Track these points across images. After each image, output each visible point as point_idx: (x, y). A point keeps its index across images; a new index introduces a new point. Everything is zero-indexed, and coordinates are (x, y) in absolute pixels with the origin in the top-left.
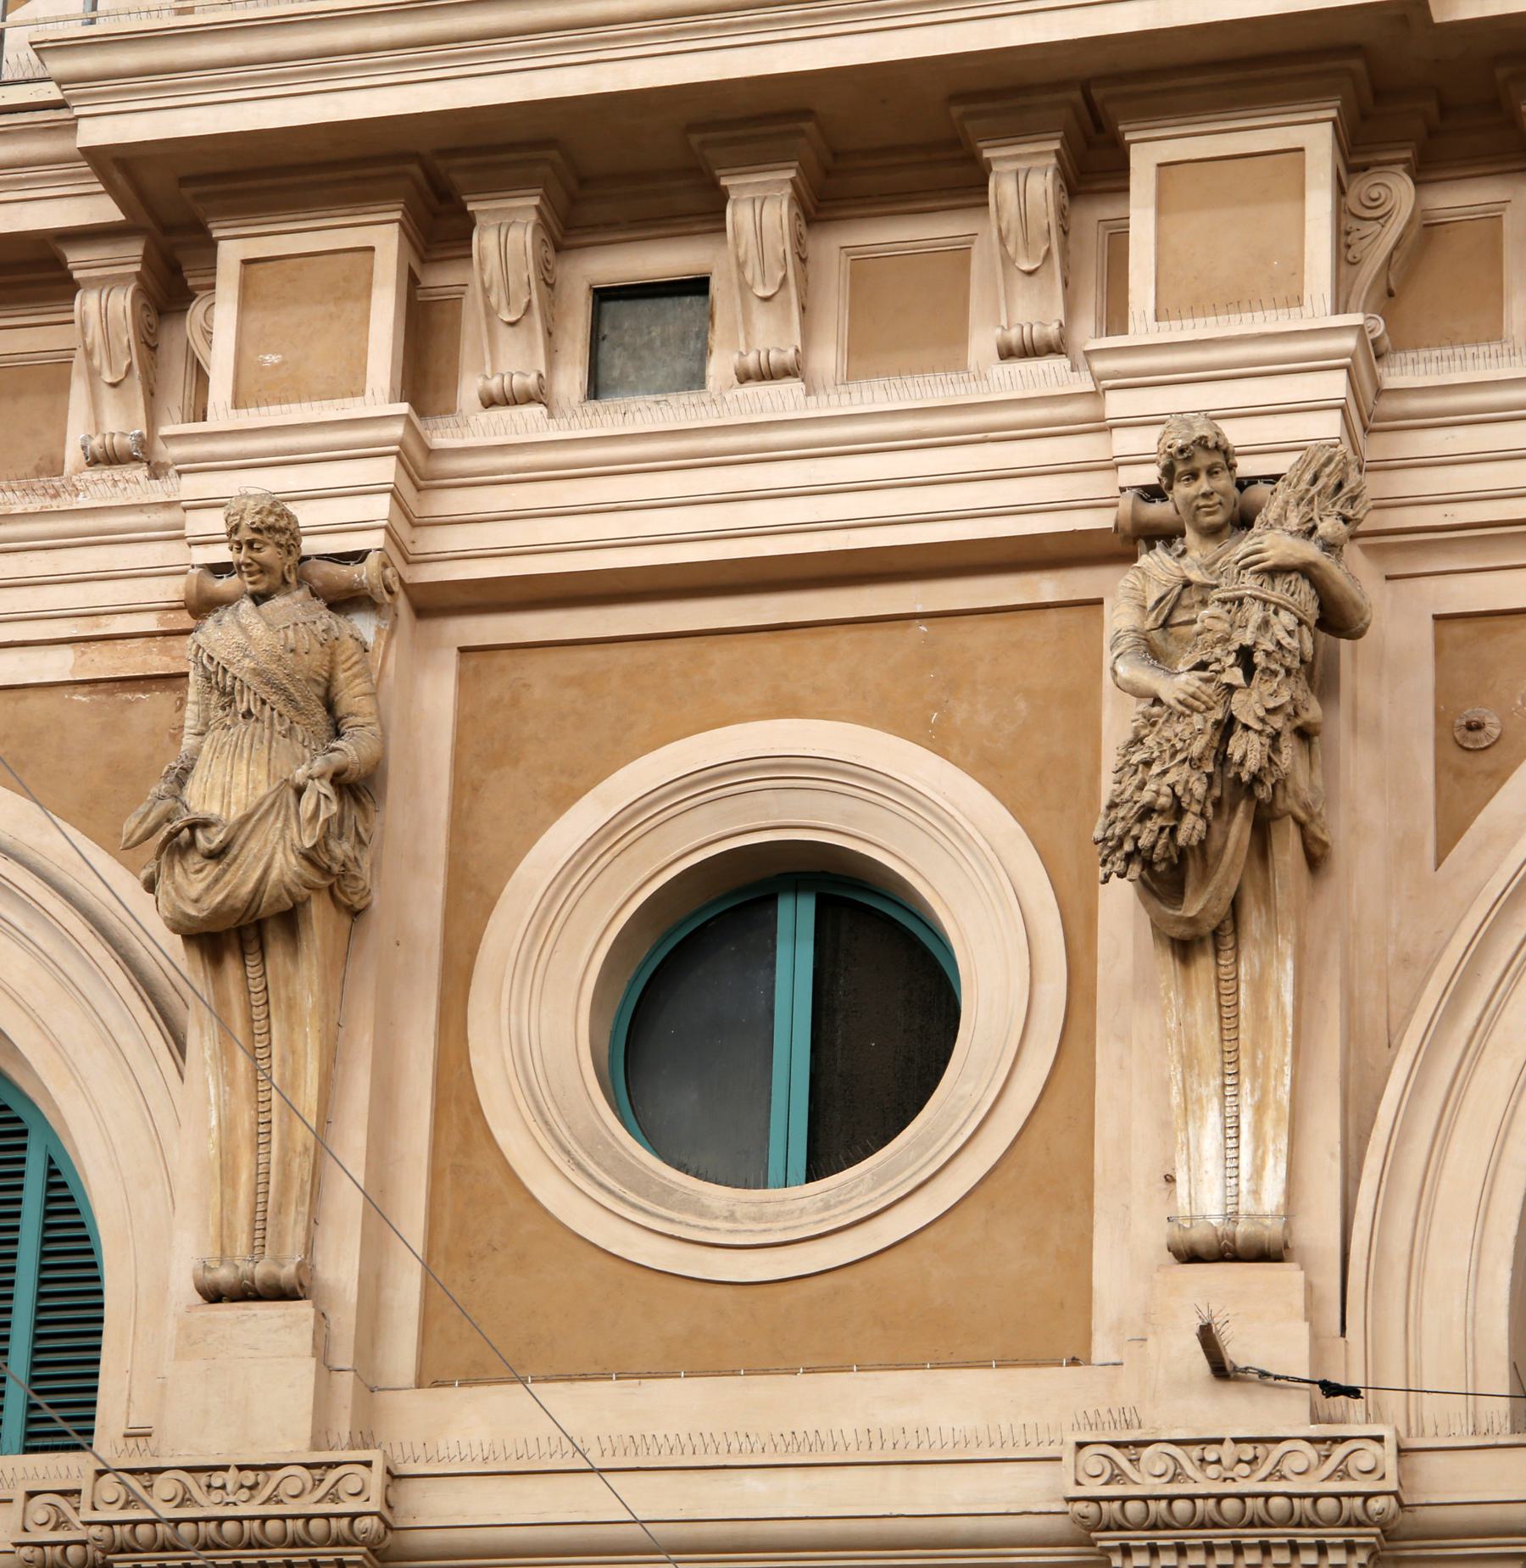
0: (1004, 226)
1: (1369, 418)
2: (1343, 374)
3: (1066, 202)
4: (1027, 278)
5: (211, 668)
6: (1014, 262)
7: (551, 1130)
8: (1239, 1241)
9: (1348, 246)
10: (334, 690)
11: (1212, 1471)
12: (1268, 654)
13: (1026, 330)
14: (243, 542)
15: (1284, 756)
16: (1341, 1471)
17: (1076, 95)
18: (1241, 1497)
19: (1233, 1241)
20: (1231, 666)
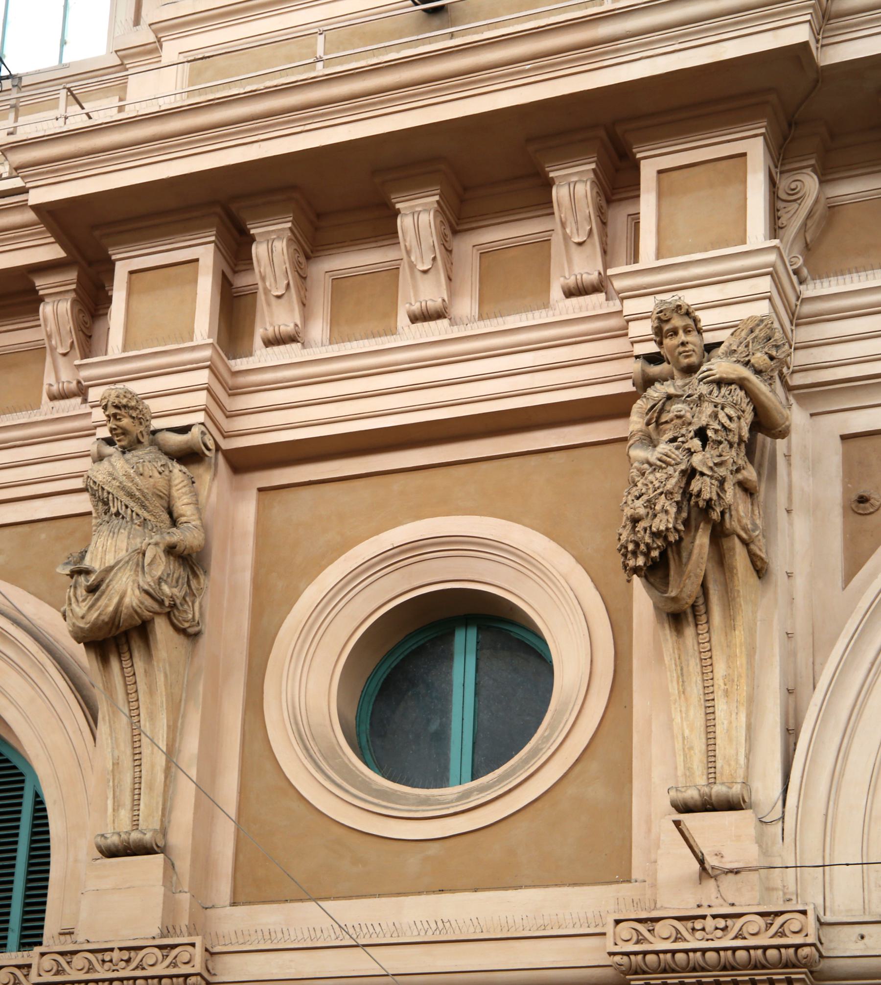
0: (407, 244)
2: (769, 278)
3: (604, 203)
4: (580, 248)
5: (95, 488)
6: (570, 238)
7: (311, 756)
8: (713, 798)
9: (779, 218)
10: (172, 503)
11: (699, 935)
12: (716, 431)
13: (579, 277)
14: (110, 415)
15: (728, 494)
16: (780, 932)
17: (602, 133)
18: (717, 950)
19: (710, 796)
20: (691, 438)
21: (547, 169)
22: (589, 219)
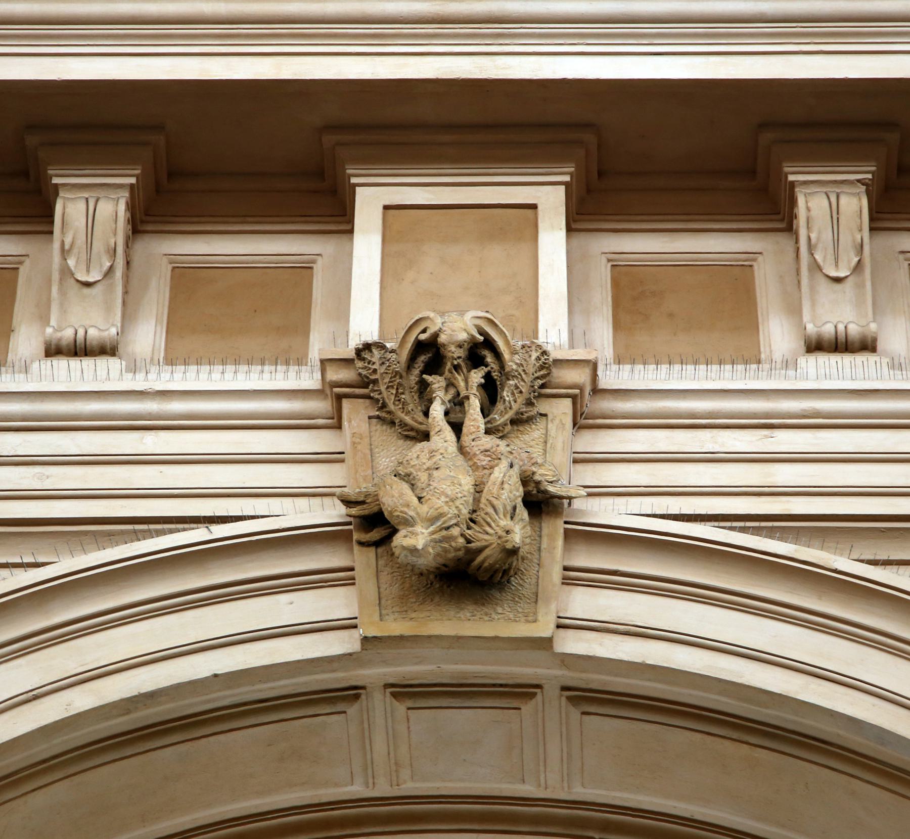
0: (813, 236)
1: (581, 415)
21: (50, 172)
22: (860, 249)
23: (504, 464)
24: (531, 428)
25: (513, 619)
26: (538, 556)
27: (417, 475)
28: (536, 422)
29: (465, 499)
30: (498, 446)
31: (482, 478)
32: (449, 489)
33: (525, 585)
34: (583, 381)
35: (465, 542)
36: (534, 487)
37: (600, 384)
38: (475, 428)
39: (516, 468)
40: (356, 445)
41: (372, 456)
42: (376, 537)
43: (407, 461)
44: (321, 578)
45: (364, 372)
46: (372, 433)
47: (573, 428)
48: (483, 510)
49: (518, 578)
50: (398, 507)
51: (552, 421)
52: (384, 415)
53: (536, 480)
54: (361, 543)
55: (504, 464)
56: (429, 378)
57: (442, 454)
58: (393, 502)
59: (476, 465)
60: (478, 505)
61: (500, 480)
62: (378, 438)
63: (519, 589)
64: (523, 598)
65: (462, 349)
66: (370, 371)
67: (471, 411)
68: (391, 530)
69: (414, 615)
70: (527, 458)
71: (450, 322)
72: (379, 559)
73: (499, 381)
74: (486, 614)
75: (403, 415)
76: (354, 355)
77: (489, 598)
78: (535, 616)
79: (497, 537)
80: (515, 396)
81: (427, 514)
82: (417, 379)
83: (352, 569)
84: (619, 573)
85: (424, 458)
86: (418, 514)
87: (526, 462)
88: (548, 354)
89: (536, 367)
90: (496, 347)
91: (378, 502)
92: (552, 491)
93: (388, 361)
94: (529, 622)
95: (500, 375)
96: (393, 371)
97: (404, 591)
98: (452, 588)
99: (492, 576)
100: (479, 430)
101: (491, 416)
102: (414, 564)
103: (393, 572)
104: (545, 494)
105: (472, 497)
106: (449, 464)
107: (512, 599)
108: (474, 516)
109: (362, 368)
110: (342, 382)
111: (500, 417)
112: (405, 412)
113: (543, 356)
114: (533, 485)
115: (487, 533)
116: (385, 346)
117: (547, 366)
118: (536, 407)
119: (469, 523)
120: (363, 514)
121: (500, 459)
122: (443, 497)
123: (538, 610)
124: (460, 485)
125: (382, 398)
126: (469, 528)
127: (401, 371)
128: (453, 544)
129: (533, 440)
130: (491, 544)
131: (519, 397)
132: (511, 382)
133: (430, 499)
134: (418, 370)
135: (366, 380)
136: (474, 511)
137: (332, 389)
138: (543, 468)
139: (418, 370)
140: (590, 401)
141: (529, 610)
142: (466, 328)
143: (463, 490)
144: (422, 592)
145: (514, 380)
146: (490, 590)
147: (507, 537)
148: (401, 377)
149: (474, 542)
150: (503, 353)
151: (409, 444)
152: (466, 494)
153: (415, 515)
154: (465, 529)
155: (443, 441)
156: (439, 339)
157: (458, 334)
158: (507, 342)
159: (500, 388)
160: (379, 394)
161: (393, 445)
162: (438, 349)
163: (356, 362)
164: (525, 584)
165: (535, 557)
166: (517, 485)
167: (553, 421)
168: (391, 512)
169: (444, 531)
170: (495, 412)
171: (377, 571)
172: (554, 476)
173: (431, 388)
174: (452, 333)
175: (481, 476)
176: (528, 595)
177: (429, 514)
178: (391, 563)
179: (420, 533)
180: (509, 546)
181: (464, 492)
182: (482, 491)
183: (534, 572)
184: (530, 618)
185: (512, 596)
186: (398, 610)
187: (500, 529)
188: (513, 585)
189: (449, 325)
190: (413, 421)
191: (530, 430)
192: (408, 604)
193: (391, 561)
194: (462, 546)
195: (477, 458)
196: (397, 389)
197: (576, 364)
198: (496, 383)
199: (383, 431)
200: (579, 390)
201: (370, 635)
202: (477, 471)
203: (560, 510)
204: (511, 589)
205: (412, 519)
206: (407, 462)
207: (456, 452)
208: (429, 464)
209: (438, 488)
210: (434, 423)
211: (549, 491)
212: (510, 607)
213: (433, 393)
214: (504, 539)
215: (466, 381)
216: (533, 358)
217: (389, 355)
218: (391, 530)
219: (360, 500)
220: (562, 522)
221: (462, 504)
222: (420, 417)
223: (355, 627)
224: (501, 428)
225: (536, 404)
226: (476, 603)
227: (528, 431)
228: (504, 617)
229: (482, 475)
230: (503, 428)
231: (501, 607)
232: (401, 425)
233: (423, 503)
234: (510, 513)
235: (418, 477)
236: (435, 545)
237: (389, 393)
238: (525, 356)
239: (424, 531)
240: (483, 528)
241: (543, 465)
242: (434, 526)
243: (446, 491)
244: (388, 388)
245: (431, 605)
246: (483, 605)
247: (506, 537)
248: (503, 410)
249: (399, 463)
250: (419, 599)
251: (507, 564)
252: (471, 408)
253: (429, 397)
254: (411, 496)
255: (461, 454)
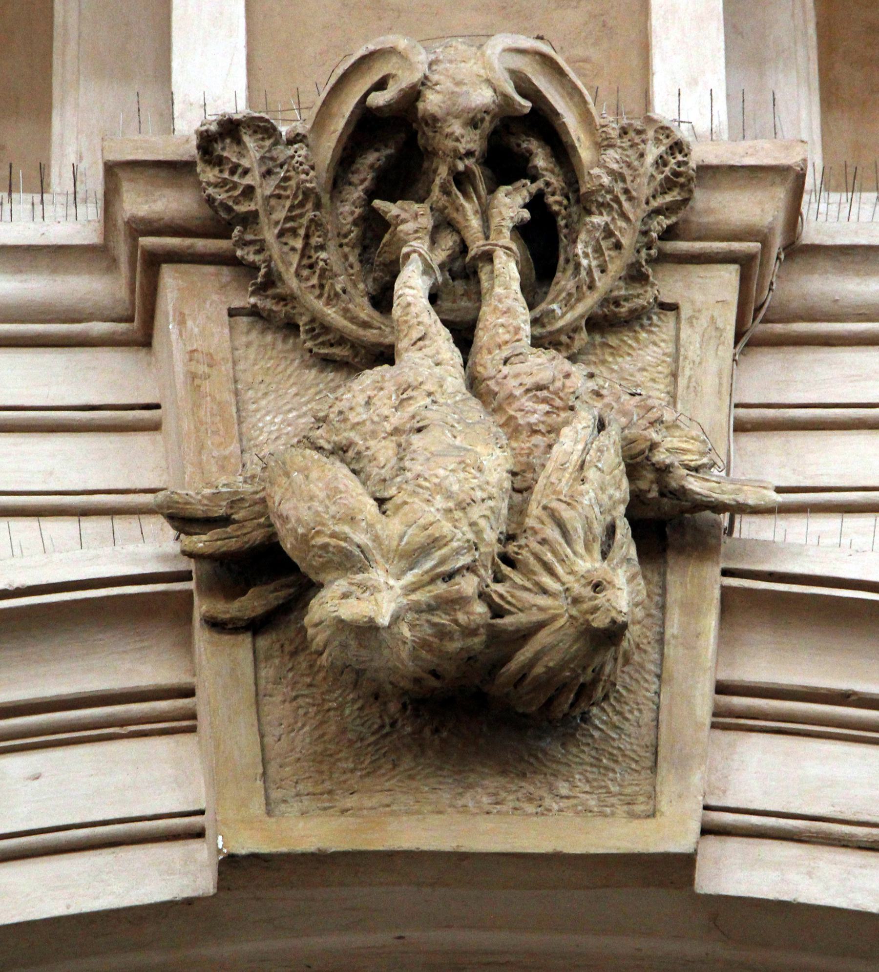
1: (758, 310)
23: (584, 420)
24: (637, 340)
25: (596, 809)
26: (657, 656)
27: (368, 448)
28: (650, 325)
29: (491, 503)
30: (567, 376)
31: (528, 455)
32: (452, 479)
33: (626, 726)
34: (770, 219)
35: (489, 615)
36: (652, 482)
37: (804, 235)
38: (509, 332)
39: (613, 433)
40: (197, 382)
41: (238, 410)
42: (255, 607)
43: (341, 413)
44: (110, 716)
45: (221, 196)
46: (237, 353)
47: (735, 347)
48: (535, 532)
49: (609, 710)
50: (324, 525)
51: (690, 320)
52: (267, 304)
53: (658, 462)
54: (215, 625)
55: (584, 420)
56: (391, 209)
57: (430, 394)
58: (311, 513)
59: (512, 424)
60: (521, 524)
61: (575, 458)
62: (254, 365)
63: (611, 737)
64: (620, 759)
65: (478, 132)
66: (237, 193)
67: (499, 290)
68: (292, 590)
69: (350, 802)
70: (636, 406)
71: (451, 62)
72: (263, 665)
73: (564, 218)
74: (530, 799)
75: (319, 305)
76: (194, 151)
77: (537, 758)
78: (652, 802)
79: (569, 600)
80: (603, 254)
81: (401, 538)
82: (358, 211)
83: (188, 692)
84: (853, 698)
85: (384, 405)
86: (376, 539)
87: (635, 418)
88: (686, 150)
89: (656, 183)
90: (558, 129)
91: (262, 520)
92: (698, 490)
93: (281, 166)
94: (638, 817)
95: (565, 202)
96: (298, 188)
97: (325, 742)
98: (445, 734)
99: (550, 702)
100: (517, 337)
101: (543, 306)
102: (362, 667)
103: (295, 698)
104: (678, 499)
105: (507, 501)
106: (449, 420)
107: (592, 760)
108: (511, 548)
109: (216, 186)
110: (162, 222)
111: (564, 309)
112: (326, 295)
113: (672, 154)
114: (650, 476)
115: (545, 591)
116: (275, 129)
117: (682, 180)
118: (653, 285)
119: (499, 566)
120: (224, 549)
121: (572, 408)
122: (438, 497)
123: (658, 789)
124: (480, 470)
125: (264, 262)
126: (498, 578)
127: (318, 190)
128: (462, 617)
129: (643, 369)
130: (554, 618)
131: (611, 258)
132: (596, 219)
133: (405, 503)
134: (361, 188)
135: (224, 215)
136: (511, 538)
137: (135, 240)
138: (678, 433)
139: (361, 188)
140: (778, 277)
141: (637, 789)
142: (490, 76)
143: (488, 483)
144: (369, 745)
145: (601, 214)
146: (540, 738)
147: (596, 598)
148: (318, 206)
149: (510, 613)
150: (577, 145)
151: (332, 380)
152: (494, 491)
153: (370, 544)
154: (489, 581)
155: (430, 362)
156: (421, 106)
157: (471, 90)
158: (586, 117)
159: (566, 237)
160: (258, 252)
161: (292, 381)
162: (412, 136)
163: (198, 169)
164: (627, 724)
165: (651, 658)
166: (616, 471)
167: (694, 321)
168: (305, 540)
169: (439, 582)
170: (550, 297)
171: (257, 695)
172: (703, 454)
173: (394, 234)
174: (457, 89)
175: (526, 451)
176: (634, 751)
177: (405, 539)
178: (290, 675)
179: (383, 586)
180: (600, 621)
181: (490, 488)
182: (529, 489)
183: (648, 694)
184: (639, 808)
185: (593, 753)
186: (311, 790)
187: (578, 581)
188: (597, 728)
189: (447, 70)
190: (345, 319)
191: (634, 345)
192: (336, 775)
193: (290, 670)
194: (482, 622)
195: (516, 405)
196: (307, 237)
197: (752, 179)
198: (555, 222)
199: (265, 346)
200: (759, 245)
201: (244, 852)
202: (517, 439)
203: (713, 541)
204: (592, 736)
205: (362, 552)
206: (341, 417)
207: (464, 390)
208: (397, 419)
209: (427, 476)
210: (408, 318)
211: (691, 490)
212: (588, 781)
213: (400, 248)
214: (585, 606)
215: (485, 216)
216: (650, 159)
217: (283, 152)
218: (292, 590)
219: (216, 515)
220: (717, 571)
221: (484, 516)
222: (365, 311)
223: (199, 834)
224: (564, 339)
225: (651, 279)
226: (504, 773)
227: (630, 346)
228: (576, 805)
229: (529, 448)
230: (569, 337)
231: (567, 781)
232: (313, 330)
233: (388, 512)
234: (599, 542)
235: (369, 453)
236: (418, 619)
237: (286, 249)
238: (627, 156)
239: (392, 582)
240: (535, 578)
241: (678, 427)
242: (416, 571)
243: (447, 483)
244: (281, 234)
245: (394, 777)
246: (523, 775)
247: (591, 599)
248: (574, 291)
249: (318, 420)
250: (362, 762)
251: (590, 670)
252: (497, 282)
253: (387, 257)
254: (361, 494)
255: (475, 396)
